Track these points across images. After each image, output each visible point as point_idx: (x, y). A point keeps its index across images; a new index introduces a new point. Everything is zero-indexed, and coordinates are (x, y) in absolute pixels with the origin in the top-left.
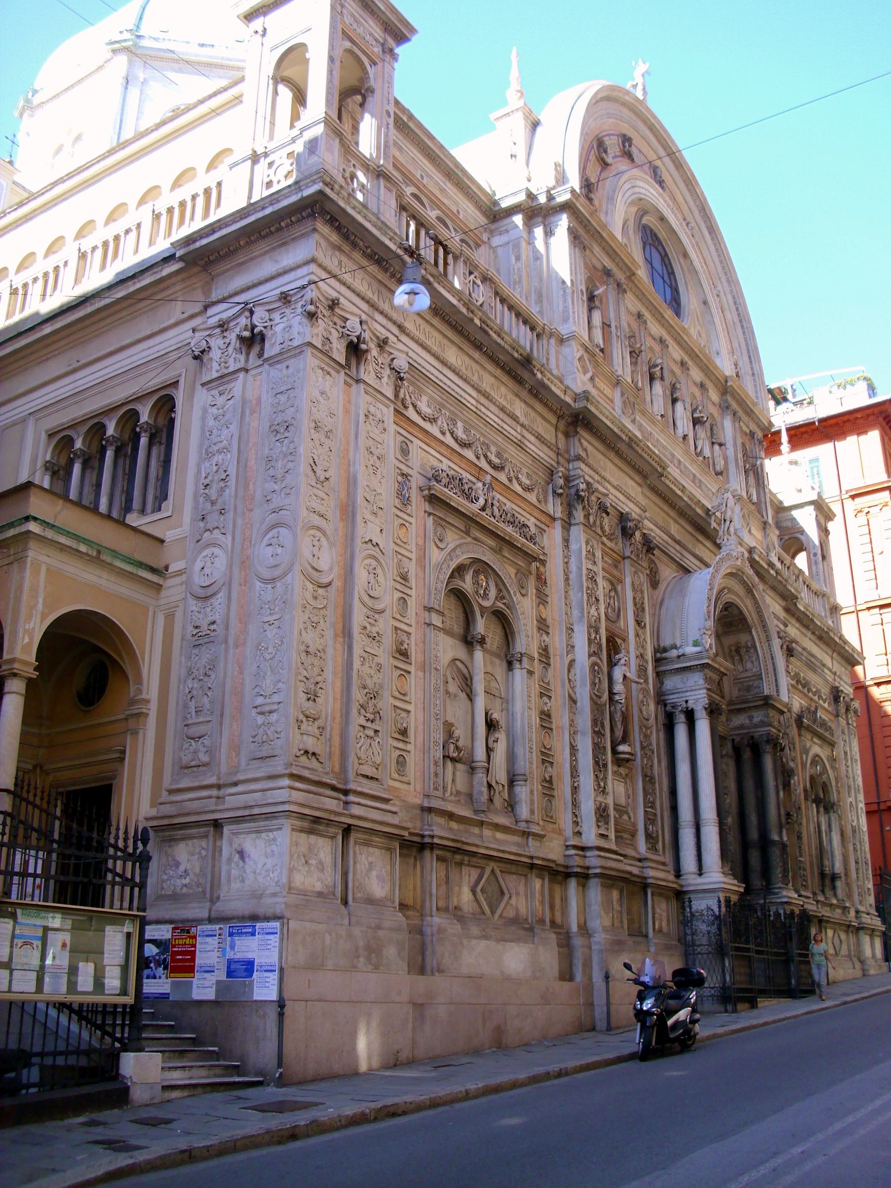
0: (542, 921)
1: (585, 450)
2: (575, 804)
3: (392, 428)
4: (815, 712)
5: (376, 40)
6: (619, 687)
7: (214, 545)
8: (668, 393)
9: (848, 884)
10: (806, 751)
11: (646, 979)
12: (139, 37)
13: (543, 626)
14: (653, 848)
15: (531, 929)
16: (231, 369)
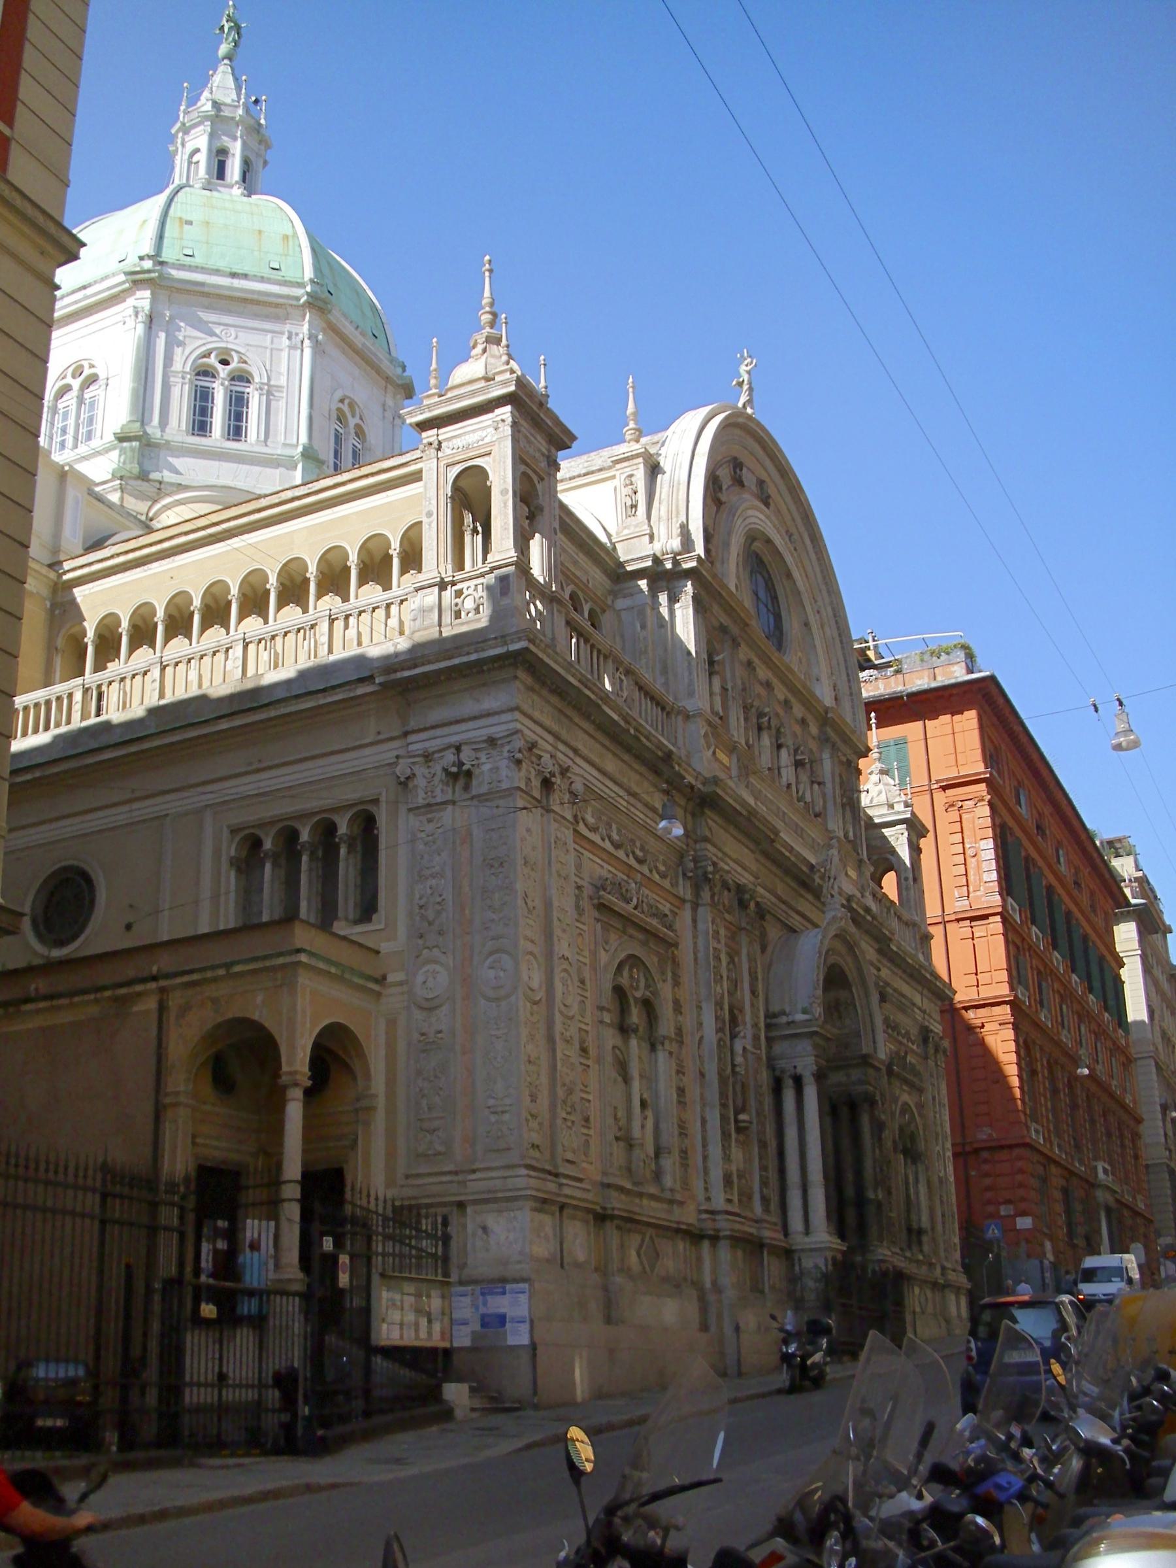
0: (685, 1279)
1: (710, 829)
2: (706, 1171)
3: (572, 845)
4: (905, 1058)
5: (543, 454)
6: (739, 1060)
7: (436, 962)
8: (774, 740)
9: (934, 1240)
10: (895, 1100)
11: (789, 1327)
12: (162, 263)
13: (678, 1007)
14: (767, 1210)
15: (678, 1286)
16: (439, 800)
